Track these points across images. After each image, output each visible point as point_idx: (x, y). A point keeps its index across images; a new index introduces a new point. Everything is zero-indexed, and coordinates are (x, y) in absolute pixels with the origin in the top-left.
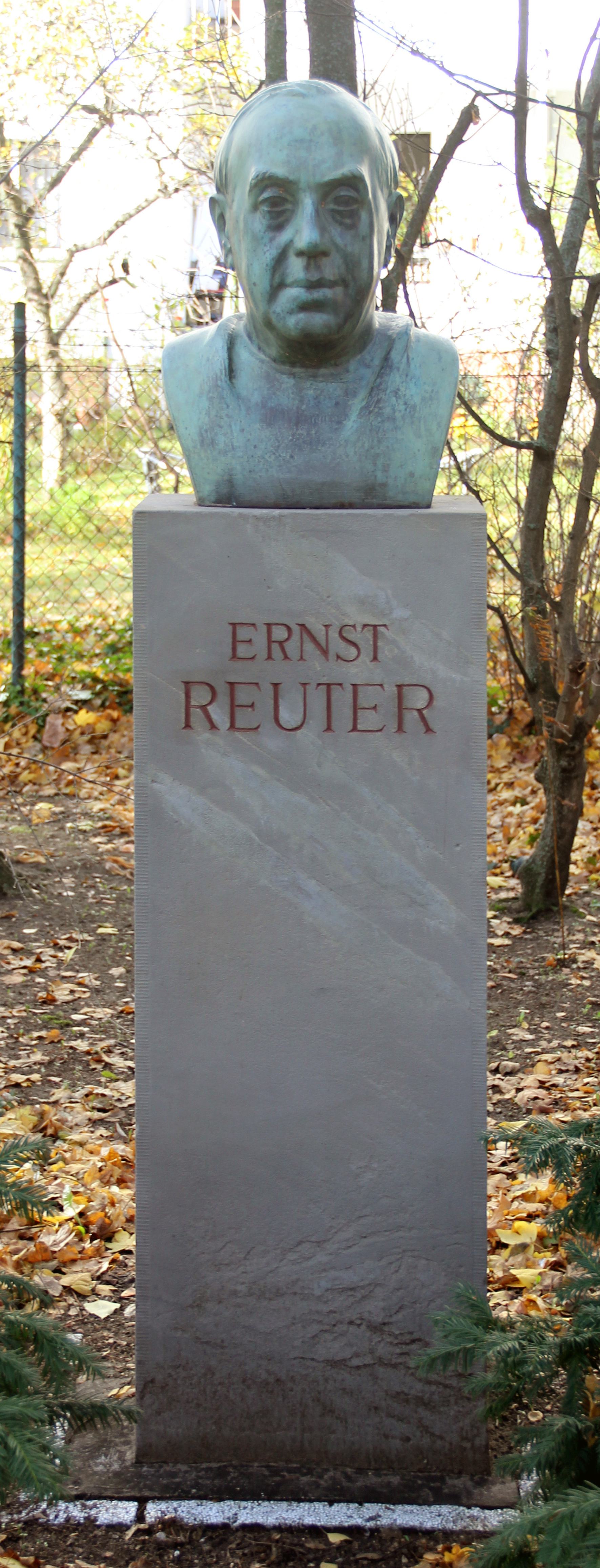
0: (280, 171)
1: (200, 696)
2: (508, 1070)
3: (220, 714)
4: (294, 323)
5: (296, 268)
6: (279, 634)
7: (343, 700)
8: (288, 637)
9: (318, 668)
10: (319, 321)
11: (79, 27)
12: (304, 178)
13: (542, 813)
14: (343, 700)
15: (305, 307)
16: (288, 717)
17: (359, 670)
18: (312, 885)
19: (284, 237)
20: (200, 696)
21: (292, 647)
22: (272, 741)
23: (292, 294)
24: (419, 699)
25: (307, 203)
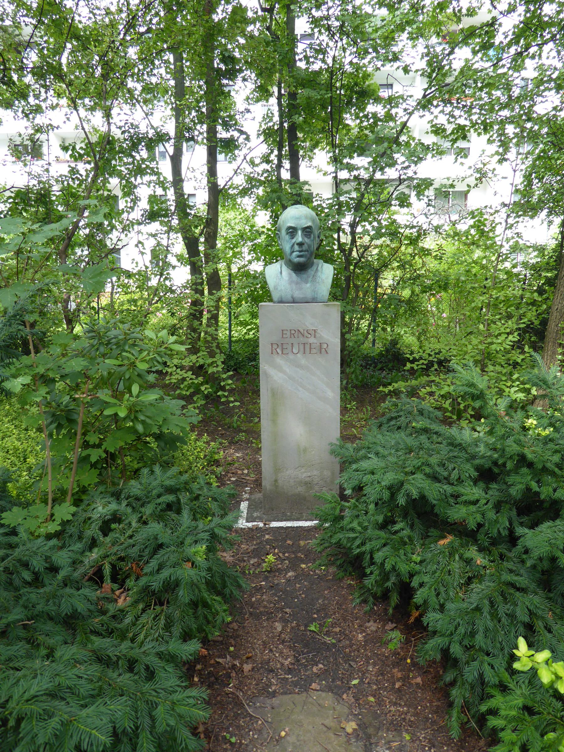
0: (293, 225)
1: (275, 346)
2: (156, 568)
3: (279, 351)
4: (297, 260)
5: (296, 248)
6: (293, 332)
7: (307, 347)
8: (297, 333)
9: (302, 340)
10: (302, 260)
11: (68, 119)
12: (299, 227)
13: (540, 275)
14: (307, 347)
15: (299, 256)
16: (295, 351)
17: (312, 340)
18: (300, 389)
19: (294, 240)
20: (275, 346)
21: (296, 335)
22: (291, 356)
23: (295, 254)
24: (325, 346)
25: (300, 232)
